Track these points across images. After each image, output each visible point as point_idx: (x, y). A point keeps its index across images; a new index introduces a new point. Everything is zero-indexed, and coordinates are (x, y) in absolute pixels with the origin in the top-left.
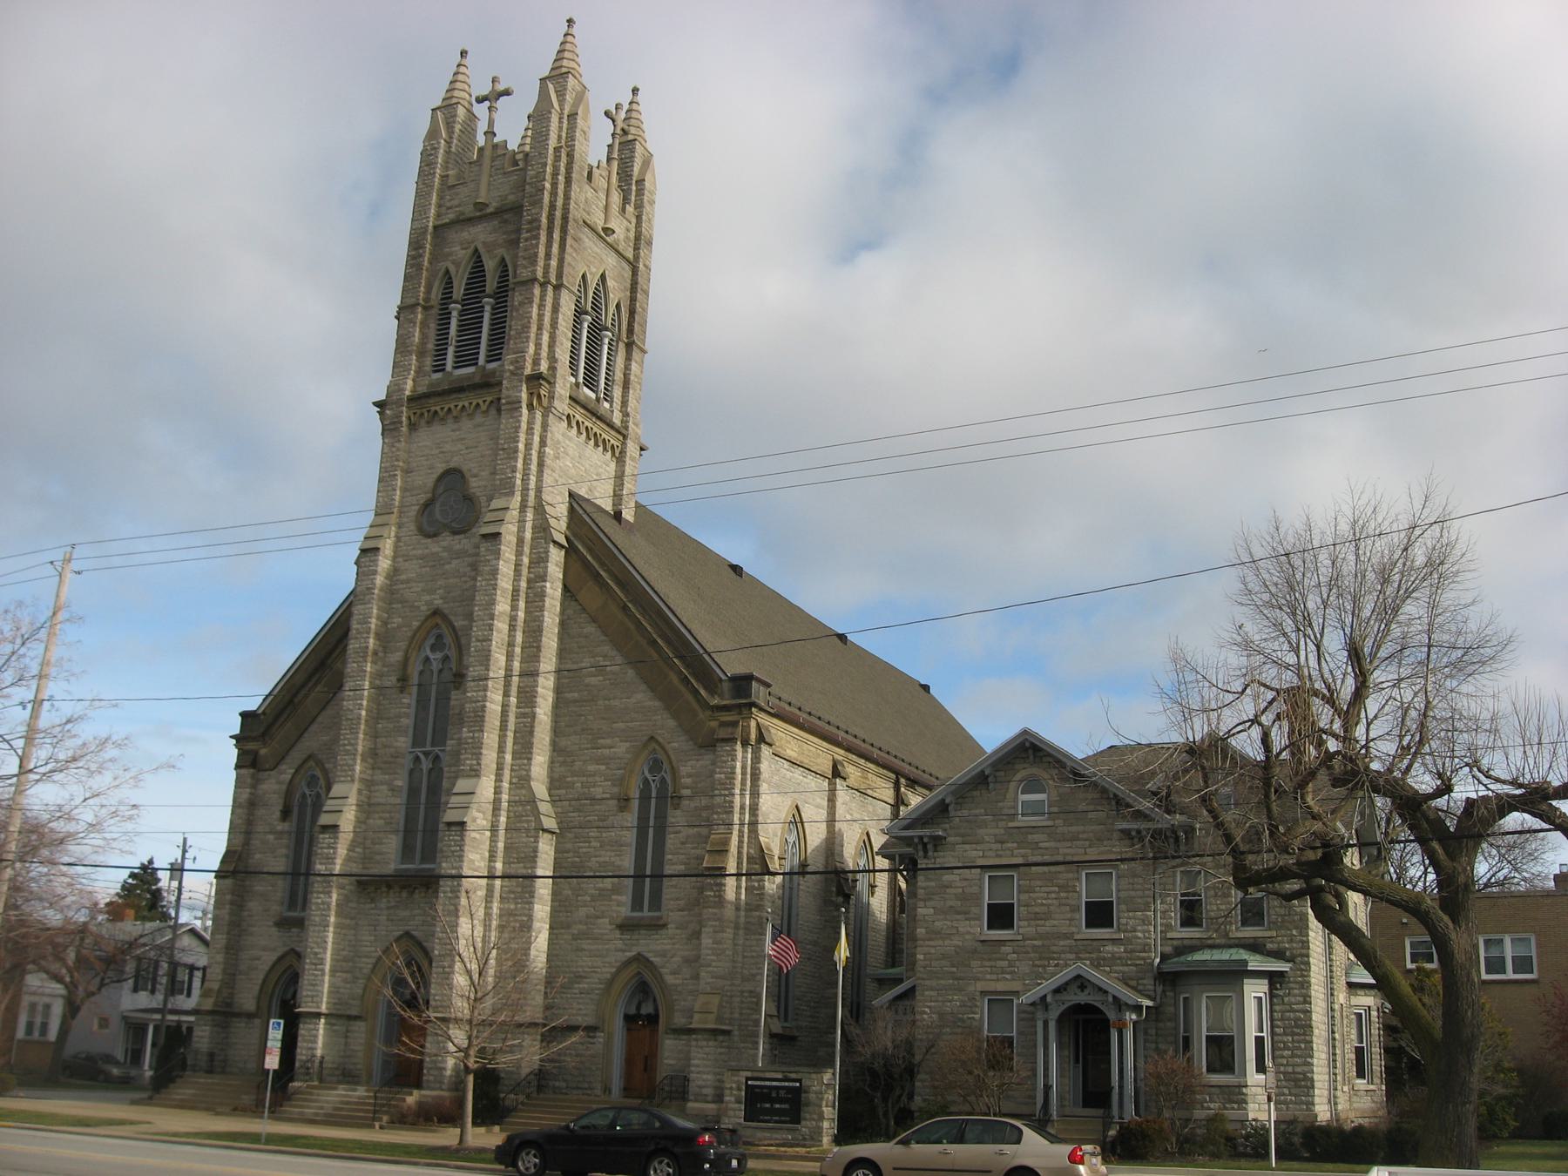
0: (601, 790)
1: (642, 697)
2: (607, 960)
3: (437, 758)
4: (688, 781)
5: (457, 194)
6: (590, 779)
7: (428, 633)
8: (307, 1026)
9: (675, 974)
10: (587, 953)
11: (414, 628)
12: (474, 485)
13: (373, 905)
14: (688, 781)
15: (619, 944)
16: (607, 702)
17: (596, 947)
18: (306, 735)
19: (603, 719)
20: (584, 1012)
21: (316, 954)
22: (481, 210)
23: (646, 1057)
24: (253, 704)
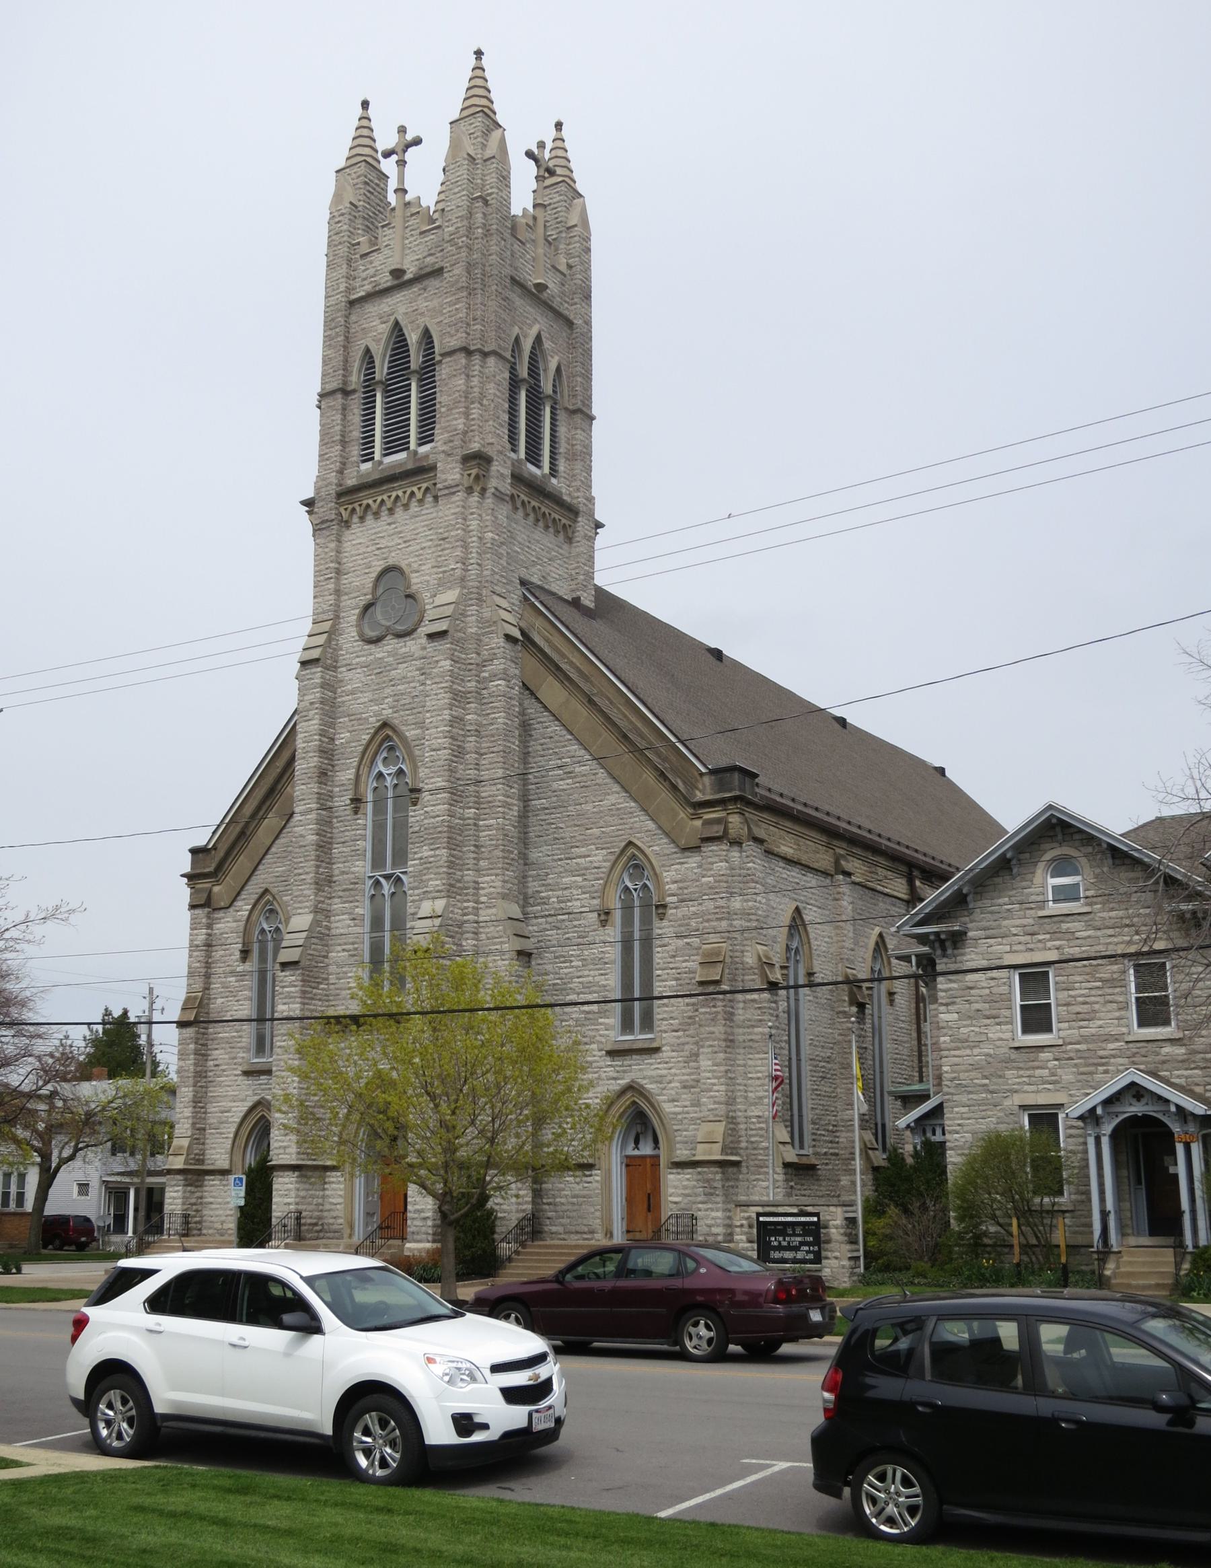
0: (578, 903)
1: (615, 798)
4: (673, 887)
5: (371, 263)
6: (566, 893)
9: (674, 1101)
11: (364, 742)
14: (673, 887)
15: (611, 1072)
18: (261, 867)
23: (649, 1195)
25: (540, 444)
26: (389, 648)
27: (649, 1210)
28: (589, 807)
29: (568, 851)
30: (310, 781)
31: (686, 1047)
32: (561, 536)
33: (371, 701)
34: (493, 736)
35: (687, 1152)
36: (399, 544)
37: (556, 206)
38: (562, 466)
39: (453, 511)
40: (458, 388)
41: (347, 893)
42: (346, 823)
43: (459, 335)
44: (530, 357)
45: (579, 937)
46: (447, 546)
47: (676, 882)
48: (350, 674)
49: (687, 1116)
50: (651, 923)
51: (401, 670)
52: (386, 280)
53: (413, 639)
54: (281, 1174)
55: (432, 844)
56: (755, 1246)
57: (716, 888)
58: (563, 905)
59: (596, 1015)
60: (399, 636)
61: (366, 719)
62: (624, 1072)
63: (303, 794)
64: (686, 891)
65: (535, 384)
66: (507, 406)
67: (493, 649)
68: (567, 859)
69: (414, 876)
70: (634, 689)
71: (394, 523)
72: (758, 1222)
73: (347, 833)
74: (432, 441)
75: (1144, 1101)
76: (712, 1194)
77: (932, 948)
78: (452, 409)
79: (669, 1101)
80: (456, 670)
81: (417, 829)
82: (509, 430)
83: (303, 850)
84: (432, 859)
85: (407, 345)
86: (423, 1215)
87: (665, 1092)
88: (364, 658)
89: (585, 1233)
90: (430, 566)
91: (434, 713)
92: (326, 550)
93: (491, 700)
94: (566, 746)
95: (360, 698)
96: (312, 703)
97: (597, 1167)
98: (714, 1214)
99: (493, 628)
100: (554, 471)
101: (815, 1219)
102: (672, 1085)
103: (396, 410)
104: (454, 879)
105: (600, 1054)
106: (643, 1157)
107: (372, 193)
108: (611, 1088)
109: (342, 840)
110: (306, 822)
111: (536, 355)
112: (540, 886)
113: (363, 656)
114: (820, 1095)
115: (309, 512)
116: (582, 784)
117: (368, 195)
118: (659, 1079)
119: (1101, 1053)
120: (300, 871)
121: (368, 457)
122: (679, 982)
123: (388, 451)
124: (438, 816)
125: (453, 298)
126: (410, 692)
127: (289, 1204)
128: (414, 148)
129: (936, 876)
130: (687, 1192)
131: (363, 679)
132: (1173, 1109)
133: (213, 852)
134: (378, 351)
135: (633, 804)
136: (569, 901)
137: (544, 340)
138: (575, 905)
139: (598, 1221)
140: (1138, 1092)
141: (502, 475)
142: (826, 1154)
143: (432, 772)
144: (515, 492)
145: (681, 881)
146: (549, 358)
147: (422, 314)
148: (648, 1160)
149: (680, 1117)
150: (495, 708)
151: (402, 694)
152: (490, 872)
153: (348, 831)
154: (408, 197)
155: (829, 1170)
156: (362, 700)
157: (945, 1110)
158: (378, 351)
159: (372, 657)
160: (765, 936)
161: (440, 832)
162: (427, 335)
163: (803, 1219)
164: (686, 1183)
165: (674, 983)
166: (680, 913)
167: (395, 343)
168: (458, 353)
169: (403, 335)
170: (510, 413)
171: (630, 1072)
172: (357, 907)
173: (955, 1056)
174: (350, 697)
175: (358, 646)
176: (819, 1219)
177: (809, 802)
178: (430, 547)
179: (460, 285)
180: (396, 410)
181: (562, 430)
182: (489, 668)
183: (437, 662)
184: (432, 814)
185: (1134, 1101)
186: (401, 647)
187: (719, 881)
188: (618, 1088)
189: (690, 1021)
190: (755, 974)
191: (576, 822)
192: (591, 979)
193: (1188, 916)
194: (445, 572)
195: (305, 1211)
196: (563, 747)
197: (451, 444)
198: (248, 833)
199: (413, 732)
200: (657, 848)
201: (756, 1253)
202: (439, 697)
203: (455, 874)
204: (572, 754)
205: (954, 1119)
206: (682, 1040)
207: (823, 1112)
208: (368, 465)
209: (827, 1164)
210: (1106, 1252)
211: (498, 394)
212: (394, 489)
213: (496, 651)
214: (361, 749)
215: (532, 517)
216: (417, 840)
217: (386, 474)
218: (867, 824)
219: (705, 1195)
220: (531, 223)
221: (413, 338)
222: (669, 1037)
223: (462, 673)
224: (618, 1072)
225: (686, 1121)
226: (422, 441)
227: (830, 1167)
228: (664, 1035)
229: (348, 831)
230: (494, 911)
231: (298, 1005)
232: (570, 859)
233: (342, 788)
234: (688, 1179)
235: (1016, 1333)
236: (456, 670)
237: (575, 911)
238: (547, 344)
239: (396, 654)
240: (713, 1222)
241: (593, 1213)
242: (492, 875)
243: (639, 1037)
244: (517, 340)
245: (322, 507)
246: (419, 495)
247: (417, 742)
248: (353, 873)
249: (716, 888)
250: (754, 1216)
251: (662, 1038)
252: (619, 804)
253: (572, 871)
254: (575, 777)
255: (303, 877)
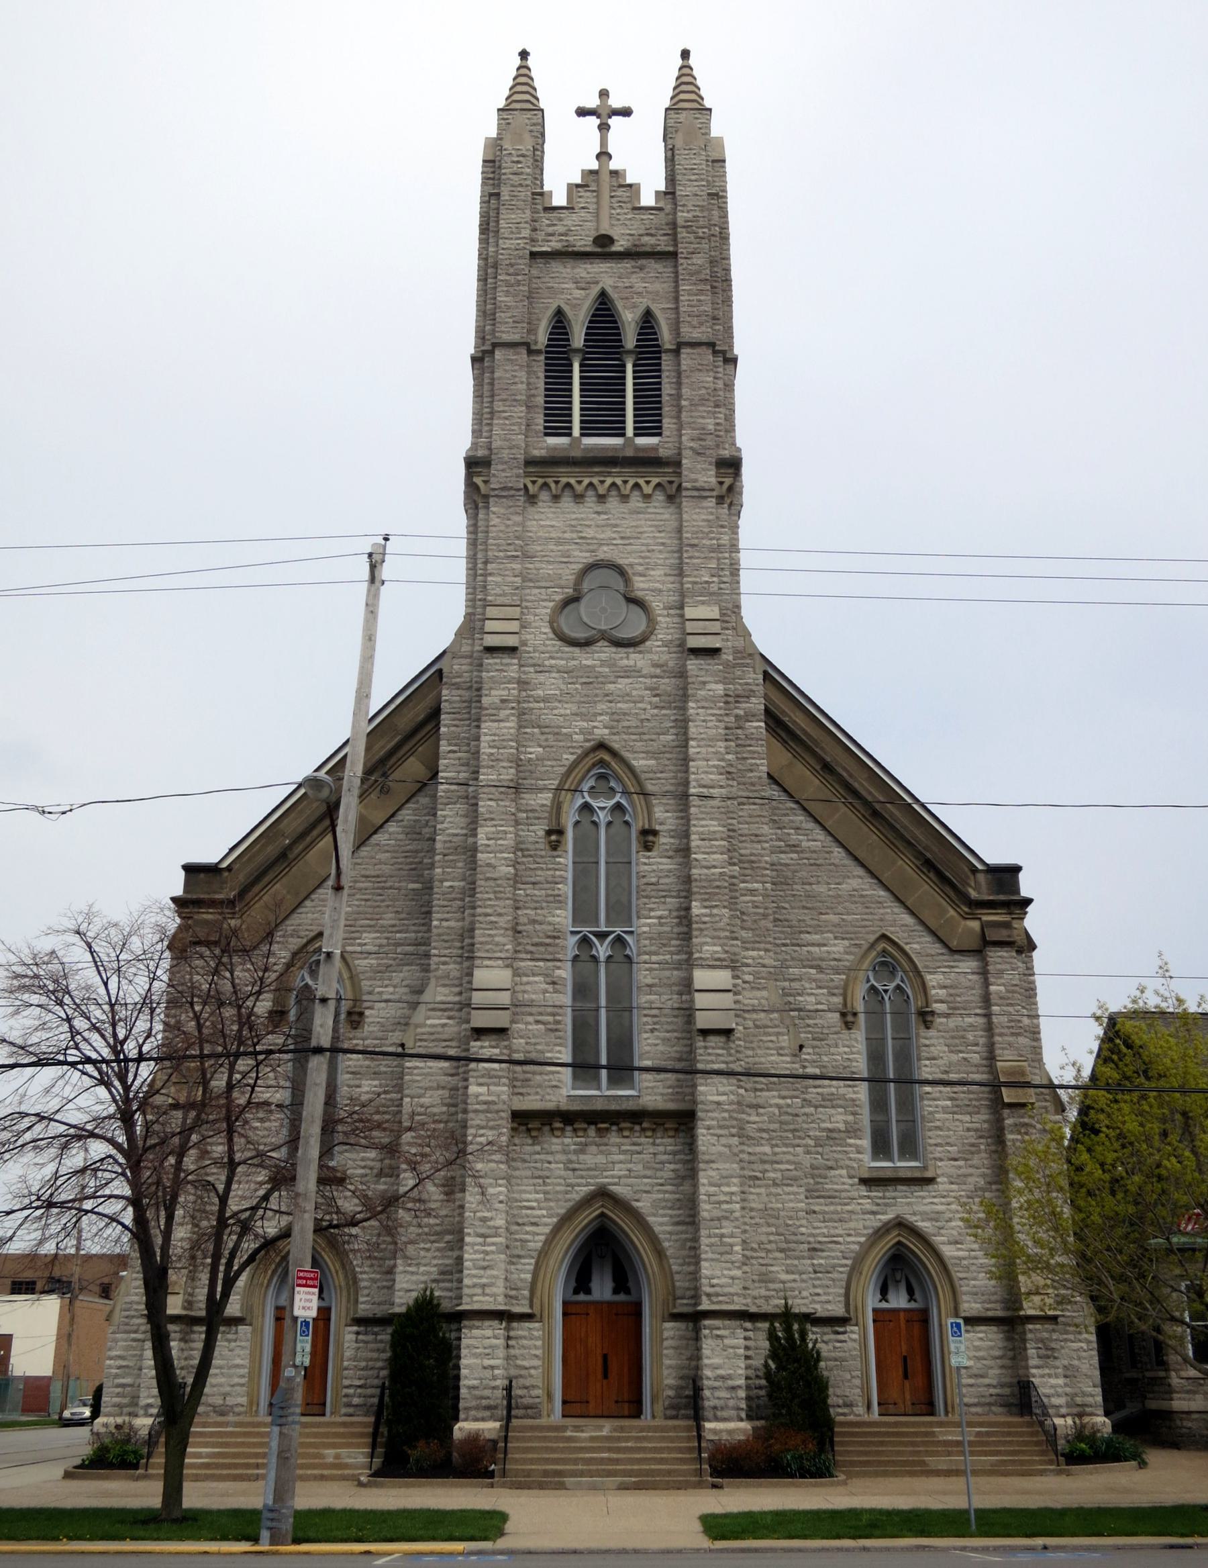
0: (812, 999)
1: (857, 882)
2: (852, 1225)
3: (620, 941)
4: (942, 993)
5: (560, 220)
6: (795, 985)
7: (589, 771)
8: (475, 1332)
9: (957, 1243)
10: (820, 1217)
11: (567, 763)
12: (642, 585)
13: (538, 1148)
14: (942, 993)
15: (867, 1204)
16: (807, 887)
17: (832, 1208)
18: (308, 903)
19: (804, 908)
20: (823, 1298)
21: (484, 1220)
22: (602, 246)
23: (905, 1358)
24: (211, 854)
26: (603, 656)
27: (906, 1376)
28: (822, 889)
29: (796, 936)
30: (502, 796)
31: (970, 1180)
33: (576, 715)
34: (753, 784)
35: (978, 1306)
39: (704, 517)
40: (707, 385)
41: (542, 949)
42: (538, 860)
43: (703, 329)
45: (814, 1039)
46: (697, 554)
47: (945, 987)
48: (542, 678)
49: (975, 1261)
50: (907, 1029)
51: (623, 684)
52: (584, 242)
53: (640, 652)
54: (477, 1323)
55: (706, 900)
57: (1009, 998)
58: (791, 999)
59: (843, 1135)
60: (619, 643)
61: (569, 736)
62: (886, 1205)
63: (491, 813)
64: (958, 999)
67: (747, 684)
68: (793, 945)
69: (651, 939)
71: (605, 513)
73: (539, 873)
76: (1048, 1357)
79: (950, 1243)
81: (654, 880)
83: (492, 883)
84: (706, 919)
86: (730, 1383)
87: (942, 1231)
88: (563, 662)
90: (662, 572)
91: (702, 743)
93: (748, 742)
94: (787, 815)
95: (556, 708)
96: (503, 701)
97: (853, 1322)
98: (1053, 1381)
102: (953, 1224)
105: (850, 1181)
106: (895, 1311)
108: (868, 1223)
109: (532, 880)
110: (498, 848)
113: (562, 659)
116: (812, 861)
118: (933, 1215)
120: (489, 911)
122: (955, 1103)
124: (715, 867)
127: (492, 1368)
128: (620, 118)
130: (981, 1354)
131: (563, 687)
133: (226, 874)
135: (882, 893)
136: (799, 994)
138: (809, 1001)
139: (859, 1390)
143: (702, 812)
145: (951, 987)
148: (902, 1314)
149: (965, 1262)
150: (754, 752)
151: (625, 714)
152: (757, 945)
153: (542, 869)
154: (613, 165)
156: (562, 712)
159: (575, 663)
161: (718, 887)
164: (977, 1343)
165: (949, 1103)
166: (952, 1022)
168: (704, 348)
171: (895, 1205)
172: (559, 968)
174: (542, 705)
175: (554, 646)
178: (660, 551)
179: (703, 277)
182: (744, 705)
183: (704, 683)
184: (705, 863)
186: (622, 658)
187: (1013, 992)
188: (879, 1224)
189: (973, 1149)
190: (1046, 1101)
191: (804, 903)
192: (834, 1090)
194: (696, 583)
196: (785, 815)
198: (291, 856)
199: (642, 762)
200: (919, 945)
202: (709, 724)
204: (798, 825)
206: (963, 1171)
212: (609, 474)
213: (754, 688)
214: (563, 770)
216: (653, 893)
219: (1039, 1357)
221: (629, 318)
222: (945, 1167)
224: (878, 1205)
225: (973, 1268)
228: (940, 1164)
229: (542, 869)
230: (765, 993)
231: (506, 1088)
232: (798, 945)
233: (530, 815)
234: (981, 1339)
235: (162, 1490)
237: (809, 1007)
239: (615, 665)
240: (1052, 1391)
241: (849, 1381)
242: (759, 950)
243: (906, 1166)
245: (503, 470)
247: (651, 775)
248: (550, 924)
249: (1009, 998)
251: (936, 1167)
252: (863, 890)
253: (802, 960)
254: (802, 852)
255: (492, 919)
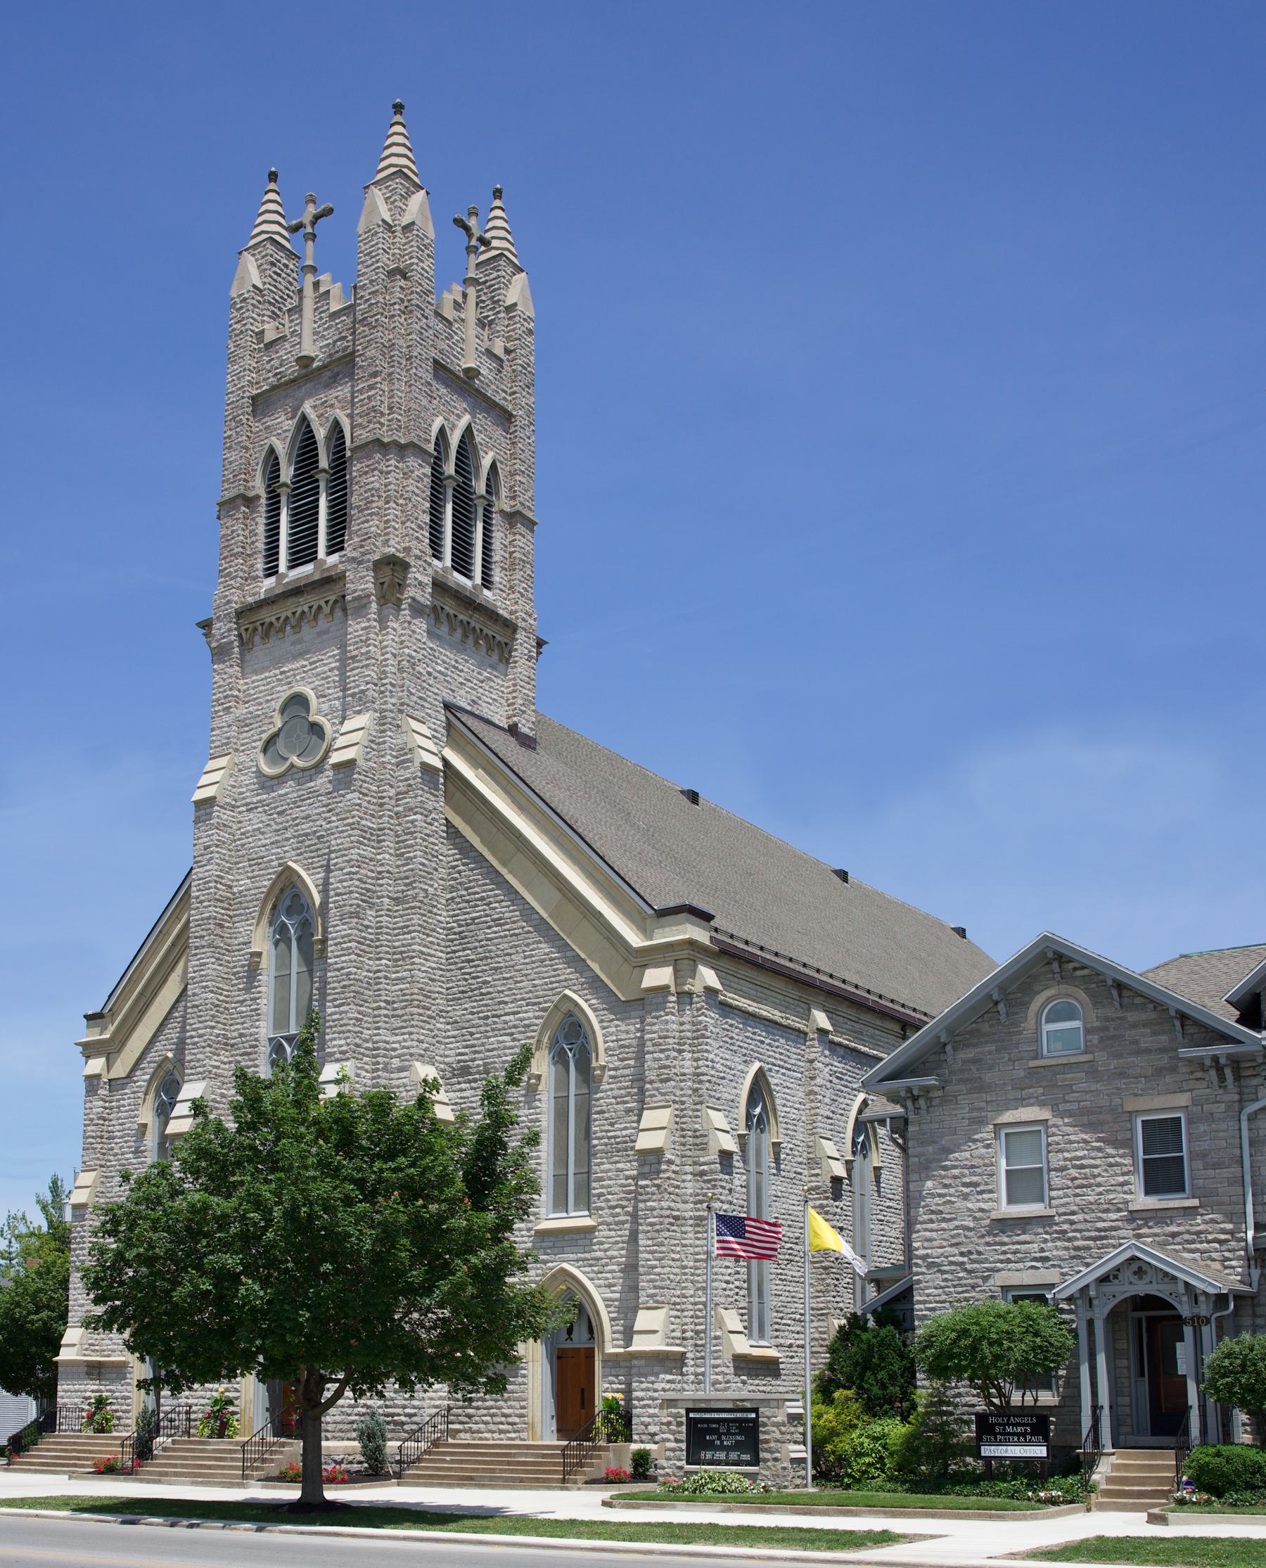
23: (583, 1390)
25: (471, 551)
32: (495, 657)
36: (305, 666)
37: (493, 282)
38: (497, 576)
44: (458, 452)
56: (684, 1446)
65: (463, 482)
66: (428, 505)
68: (494, 1016)
70: (571, 822)
72: (689, 1420)
74: (342, 549)
75: (1147, 1279)
77: (904, 1106)
78: (363, 510)
80: (365, 804)
82: (431, 534)
85: (315, 443)
89: (510, 1432)
92: (225, 676)
99: (409, 756)
100: (487, 582)
101: (753, 1415)
103: (305, 518)
104: (361, 1038)
107: (279, 275)
111: (466, 451)
112: (464, 1048)
114: (785, 1280)
115: (206, 635)
117: (275, 277)
119: (1100, 1225)
121: (272, 571)
123: (294, 563)
125: (366, 384)
126: (315, 832)
129: (906, 1025)
132: (1181, 1289)
134: (281, 448)
137: (475, 433)
140: (1140, 1268)
141: (420, 583)
142: (790, 1346)
144: (438, 603)
146: (482, 453)
147: (332, 406)
152: (403, 1031)
155: (795, 1363)
157: (915, 1293)
158: (281, 448)
160: (718, 1099)
162: (336, 427)
163: (739, 1415)
167: (302, 441)
169: (311, 431)
170: (431, 514)
173: (926, 1230)
176: (758, 1416)
177: (822, 968)
180: (305, 518)
181: (498, 536)
185: (1134, 1279)
193: (1208, 1062)
195: (196, 1405)
197: (362, 550)
201: (685, 1453)
203: (362, 1033)
205: (925, 1302)
207: (789, 1299)
208: (273, 579)
209: (792, 1357)
210: (1097, 1454)
211: (417, 491)
213: (412, 782)
215: (459, 631)
217: (290, 587)
218: (855, 979)
220: (460, 300)
221: (321, 433)
223: (372, 807)
226: (331, 550)
227: (796, 1360)
236: (365, 804)
238: (479, 438)
242: (404, 1034)
244: (442, 431)
246: (326, 609)
250: (683, 1412)
